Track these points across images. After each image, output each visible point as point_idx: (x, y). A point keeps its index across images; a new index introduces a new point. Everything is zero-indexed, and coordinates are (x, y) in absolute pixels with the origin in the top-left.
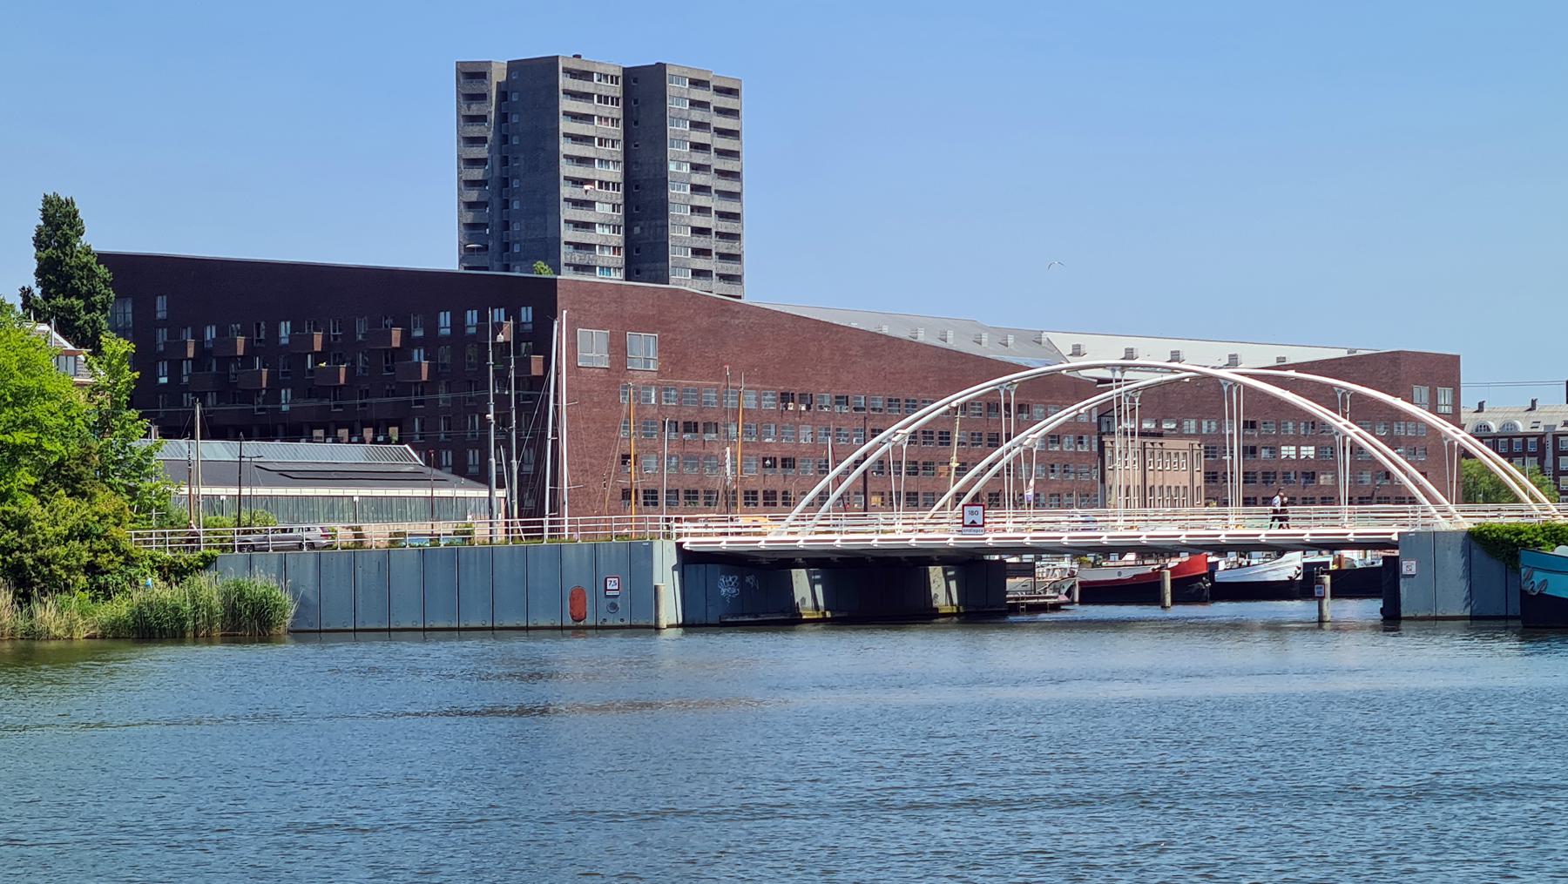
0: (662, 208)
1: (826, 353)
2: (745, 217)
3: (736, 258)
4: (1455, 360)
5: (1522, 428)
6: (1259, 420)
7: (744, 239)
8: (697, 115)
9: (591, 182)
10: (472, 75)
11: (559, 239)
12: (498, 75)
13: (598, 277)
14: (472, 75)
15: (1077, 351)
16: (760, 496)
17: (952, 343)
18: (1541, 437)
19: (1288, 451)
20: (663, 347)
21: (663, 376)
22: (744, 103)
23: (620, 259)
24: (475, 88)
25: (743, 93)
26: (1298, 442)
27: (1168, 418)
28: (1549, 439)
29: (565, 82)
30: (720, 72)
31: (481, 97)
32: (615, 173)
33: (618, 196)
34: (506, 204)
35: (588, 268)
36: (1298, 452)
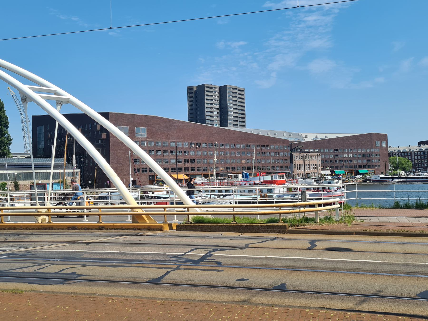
0: (226, 112)
1: (205, 133)
2: (246, 114)
3: (244, 122)
4: (386, 135)
5: (407, 151)
6: (338, 149)
7: (246, 119)
8: (234, 95)
9: (212, 108)
10: (190, 89)
11: (205, 119)
12: (195, 89)
13: (215, 126)
14: (190, 89)
15: (306, 137)
16: (183, 169)
17: (270, 135)
18: (411, 152)
19: (346, 156)
20: (148, 131)
21: (149, 138)
22: (245, 93)
23: (219, 122)
24: (191, 91)
25: (245, 91)
26: (348, 153)
27: (317, 149)
28: (413, 153)
29: (206, 89)
30: (239, 86)
31: (192, 93)
32: (218, 106)
33: (218, 111)
34: (197, 113)
35: (213, 125)
36: (348, 156)
